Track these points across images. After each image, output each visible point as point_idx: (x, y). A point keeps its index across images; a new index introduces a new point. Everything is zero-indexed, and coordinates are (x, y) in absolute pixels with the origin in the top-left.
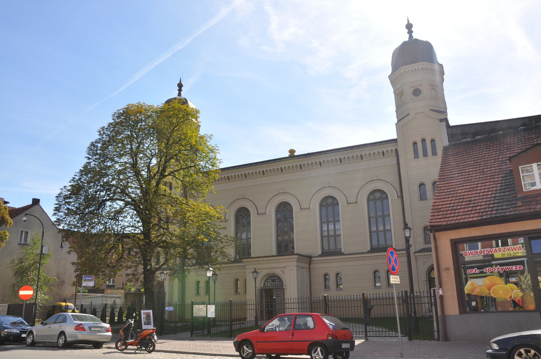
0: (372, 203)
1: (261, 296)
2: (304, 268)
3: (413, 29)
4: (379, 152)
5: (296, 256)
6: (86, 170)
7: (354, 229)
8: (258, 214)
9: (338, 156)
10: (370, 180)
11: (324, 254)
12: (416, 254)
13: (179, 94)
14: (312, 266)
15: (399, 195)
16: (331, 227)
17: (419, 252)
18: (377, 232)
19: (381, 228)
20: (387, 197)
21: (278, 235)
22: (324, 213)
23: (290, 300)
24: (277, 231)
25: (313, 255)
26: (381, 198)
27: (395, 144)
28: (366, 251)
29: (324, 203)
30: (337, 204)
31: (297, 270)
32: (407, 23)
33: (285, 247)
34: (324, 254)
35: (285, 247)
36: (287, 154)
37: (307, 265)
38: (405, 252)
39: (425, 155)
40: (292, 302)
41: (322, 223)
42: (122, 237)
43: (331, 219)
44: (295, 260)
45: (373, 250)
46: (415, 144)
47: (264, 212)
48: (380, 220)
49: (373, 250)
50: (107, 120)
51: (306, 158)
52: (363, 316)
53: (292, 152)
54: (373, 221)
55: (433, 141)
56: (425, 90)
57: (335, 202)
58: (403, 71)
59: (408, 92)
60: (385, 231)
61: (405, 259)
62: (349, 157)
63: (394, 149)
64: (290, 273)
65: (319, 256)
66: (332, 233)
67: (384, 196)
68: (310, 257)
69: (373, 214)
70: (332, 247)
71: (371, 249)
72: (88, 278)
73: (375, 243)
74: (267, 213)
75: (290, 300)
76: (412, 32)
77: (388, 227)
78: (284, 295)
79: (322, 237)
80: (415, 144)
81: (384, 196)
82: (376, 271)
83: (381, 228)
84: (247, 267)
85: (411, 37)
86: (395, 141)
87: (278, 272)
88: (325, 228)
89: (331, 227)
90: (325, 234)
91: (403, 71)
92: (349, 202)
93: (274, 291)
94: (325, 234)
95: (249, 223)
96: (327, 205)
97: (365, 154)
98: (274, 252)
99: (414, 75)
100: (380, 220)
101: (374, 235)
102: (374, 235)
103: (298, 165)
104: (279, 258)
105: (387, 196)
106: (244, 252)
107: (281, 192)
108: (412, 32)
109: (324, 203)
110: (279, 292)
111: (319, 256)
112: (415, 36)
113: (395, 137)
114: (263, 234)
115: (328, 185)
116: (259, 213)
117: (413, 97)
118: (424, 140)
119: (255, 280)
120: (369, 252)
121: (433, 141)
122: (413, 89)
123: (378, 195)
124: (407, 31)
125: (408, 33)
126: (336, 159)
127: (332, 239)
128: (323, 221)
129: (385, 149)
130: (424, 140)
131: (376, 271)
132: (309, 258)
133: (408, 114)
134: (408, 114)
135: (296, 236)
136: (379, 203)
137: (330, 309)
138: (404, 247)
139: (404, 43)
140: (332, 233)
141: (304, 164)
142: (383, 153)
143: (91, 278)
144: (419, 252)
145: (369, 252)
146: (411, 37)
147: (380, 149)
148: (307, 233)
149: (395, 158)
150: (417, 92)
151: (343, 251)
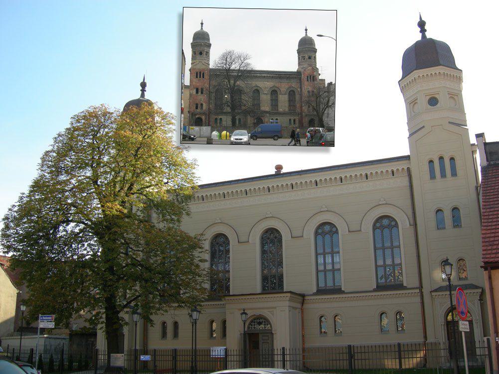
0: (378, 231)
1: (245, 341)
2: (296, 308)
3: (426, 27)
4: (336, 178)
5: (289, 295)
6: (37, 186)
7: (356, 261)
8: (349, 231)
9: (338, 174)
10: (265, 217)
11: (320, 292)
12: (433, 294)
13: (143, 95)
14: (305, 306)
15: (412, 222)
16: (329, 259)
17: (436, 291)
18: (385, 266)
19: (389, 262)
20: (396, 225)
21: (263, 267)
22: (320, 243)
23: (201, 352)
24: (263, 264)
25: (306, 293)
26: (331, 231)
27: (407, 161)
28: (372, 289)
29: (378, 225)
30: (337, 232)
31: (290, 311)
32: (419, 20)
33: (272, 283)
34: (320, 292)
35: (272, 283)
36: (273, 171)
37: (299, 306)
38: (418, 291)
39: (443, 175)
40: (165, 354)
41: (317, 255)
42: (82, 264)
43: (328, 250)
44: (288, 298)
45: (379, 288)
46: (431, 162)
47: (300, 234)
48: (388, 252)
49: (379, 288)
50: (63, 124)
51: (299, 176)
52: (348, 368)
53: (279, 168)
54: (379, 252)
55: (452, 159)
56: (442, 98)
57: (334, 229)
58: (416, 76)
59: (423, 101)
60: (394, 265)
61: (418, 299)
62: (382, 172)
63: (406, 168)
64: (280, 316)
65: (314, 294)
66: (329, 267)
67: (393, 223)
68: (303, 296)
69: (379, 245)
70: (330, 284)
71: (377, 286)
72: (46, 318)
73: (322, 285)
74: (362, 230)
75: (201, 352)
76: (426, 31)
77: (397, 261)
78: (273, 341)
79: (318, 271)
80: (431, 162)
81: (393, 223)
82: (383, 313)
83: (389, 262)
84: (227, 306)
85: (424, 36)
86: (407, 158)
87: (266, 313)
88: (321, 260)
89: (329, 259)
90: (321, 268)
91: (416, 76)
92: (293, 235)
93: (260, 336)
94: (321, 268)
95: (228, 251)
96: (324, 234)
97: (321, 180)
98: (259, 289)
99: (430, 80)
100: (388, 252)
101: (321, 275)
102: (321, 275)
103: (289, 184)
104: (264, 296)
105: (396, 223)
106: (220, 288)
107: (267, 216)
108: (426, 31)
109: (378, 225)
110: (267, 338)
111: (314, 294)
112: (429, 35)
113: (406, 152)
114: (245, 267)
115: (385, 202)
116: (240, 241)
117: (430, 107)
118: (441, 158)
119: (244, 324)
120: (374, 290)
121: (452, 159)
122: (428, 98)
123: (327, 228)
124: (419, 29)
125: (421, 32)
126: (336, 178)
127: (329, 275)
128: (318, 252)
129: (394, 166)
130: (441, 158)
131: (383, 313)
132: (302, 297)
133: (424, 127)
134: (424, 127)
135: (285, 270)
136: (386, 231)
137: (356, 361)
138: (417, 285)
139: (417, 44)
140: (329, 267)
141: (321, 180)
142: (393, 172)
143: (50, 318)
144: (436, 291)
145: (374, 290)
146: (424, 36)
147: (390, 167)
148: (299, 265)
149: (407, 179)
150: (433, 101)
151: (405, 285)
